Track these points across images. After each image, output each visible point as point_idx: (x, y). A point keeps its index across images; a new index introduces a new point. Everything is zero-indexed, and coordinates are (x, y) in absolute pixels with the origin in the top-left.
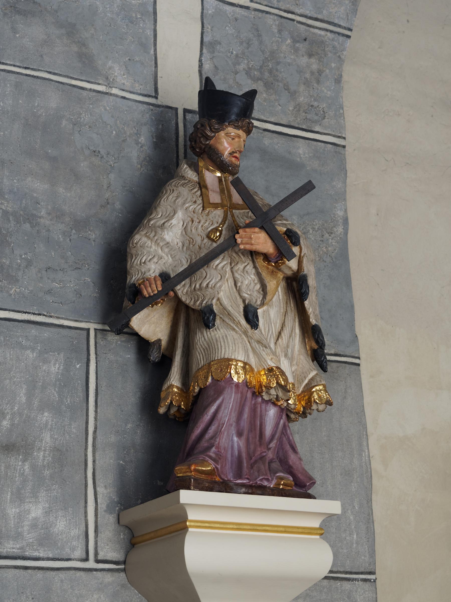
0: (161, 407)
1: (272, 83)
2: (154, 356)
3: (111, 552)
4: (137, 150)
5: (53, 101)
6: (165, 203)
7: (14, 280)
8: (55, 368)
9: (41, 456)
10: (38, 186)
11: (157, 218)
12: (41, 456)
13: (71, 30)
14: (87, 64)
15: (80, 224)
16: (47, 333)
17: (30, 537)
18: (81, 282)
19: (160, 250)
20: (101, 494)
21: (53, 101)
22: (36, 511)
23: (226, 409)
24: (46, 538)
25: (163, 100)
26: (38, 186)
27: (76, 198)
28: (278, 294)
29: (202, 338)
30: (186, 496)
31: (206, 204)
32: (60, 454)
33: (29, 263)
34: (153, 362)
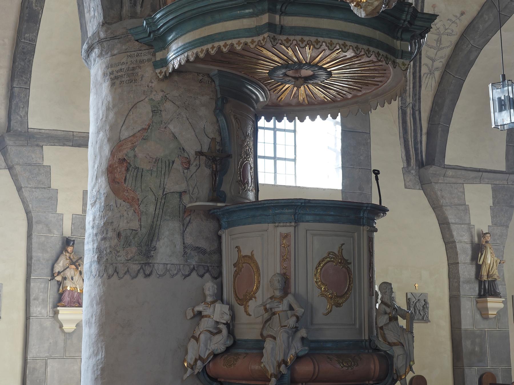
0: (451, 42)
1: (246, 44)
2: (59, 283)
3: (51, 315)
4: (58, 246)
5: (43, 239)
6: (60, 258)
7: (36, 271)
8: (43, 286)
9: (40, 300)
10: (40, 255)
11: (58, 261)
12: (40, 300)
13: (47, 225)
14: (50, 231)
15: (48, 260)
16: (41, 280)
17: (38, 313)
18: (48, 271)
19: (58, 268)
20: (50, 306)
21: (43, 239)
22: (39, 309)
23: (66, 294)
24: (41, 313)
25: (64, 235)
26: (40, 255)
27: (47, 256)
28: (78, 274)
29: (65, 282)
30: (58, 308)
31: (67, 259)
32: (43, 300)
33: (39, 268)
34: (59, 283)
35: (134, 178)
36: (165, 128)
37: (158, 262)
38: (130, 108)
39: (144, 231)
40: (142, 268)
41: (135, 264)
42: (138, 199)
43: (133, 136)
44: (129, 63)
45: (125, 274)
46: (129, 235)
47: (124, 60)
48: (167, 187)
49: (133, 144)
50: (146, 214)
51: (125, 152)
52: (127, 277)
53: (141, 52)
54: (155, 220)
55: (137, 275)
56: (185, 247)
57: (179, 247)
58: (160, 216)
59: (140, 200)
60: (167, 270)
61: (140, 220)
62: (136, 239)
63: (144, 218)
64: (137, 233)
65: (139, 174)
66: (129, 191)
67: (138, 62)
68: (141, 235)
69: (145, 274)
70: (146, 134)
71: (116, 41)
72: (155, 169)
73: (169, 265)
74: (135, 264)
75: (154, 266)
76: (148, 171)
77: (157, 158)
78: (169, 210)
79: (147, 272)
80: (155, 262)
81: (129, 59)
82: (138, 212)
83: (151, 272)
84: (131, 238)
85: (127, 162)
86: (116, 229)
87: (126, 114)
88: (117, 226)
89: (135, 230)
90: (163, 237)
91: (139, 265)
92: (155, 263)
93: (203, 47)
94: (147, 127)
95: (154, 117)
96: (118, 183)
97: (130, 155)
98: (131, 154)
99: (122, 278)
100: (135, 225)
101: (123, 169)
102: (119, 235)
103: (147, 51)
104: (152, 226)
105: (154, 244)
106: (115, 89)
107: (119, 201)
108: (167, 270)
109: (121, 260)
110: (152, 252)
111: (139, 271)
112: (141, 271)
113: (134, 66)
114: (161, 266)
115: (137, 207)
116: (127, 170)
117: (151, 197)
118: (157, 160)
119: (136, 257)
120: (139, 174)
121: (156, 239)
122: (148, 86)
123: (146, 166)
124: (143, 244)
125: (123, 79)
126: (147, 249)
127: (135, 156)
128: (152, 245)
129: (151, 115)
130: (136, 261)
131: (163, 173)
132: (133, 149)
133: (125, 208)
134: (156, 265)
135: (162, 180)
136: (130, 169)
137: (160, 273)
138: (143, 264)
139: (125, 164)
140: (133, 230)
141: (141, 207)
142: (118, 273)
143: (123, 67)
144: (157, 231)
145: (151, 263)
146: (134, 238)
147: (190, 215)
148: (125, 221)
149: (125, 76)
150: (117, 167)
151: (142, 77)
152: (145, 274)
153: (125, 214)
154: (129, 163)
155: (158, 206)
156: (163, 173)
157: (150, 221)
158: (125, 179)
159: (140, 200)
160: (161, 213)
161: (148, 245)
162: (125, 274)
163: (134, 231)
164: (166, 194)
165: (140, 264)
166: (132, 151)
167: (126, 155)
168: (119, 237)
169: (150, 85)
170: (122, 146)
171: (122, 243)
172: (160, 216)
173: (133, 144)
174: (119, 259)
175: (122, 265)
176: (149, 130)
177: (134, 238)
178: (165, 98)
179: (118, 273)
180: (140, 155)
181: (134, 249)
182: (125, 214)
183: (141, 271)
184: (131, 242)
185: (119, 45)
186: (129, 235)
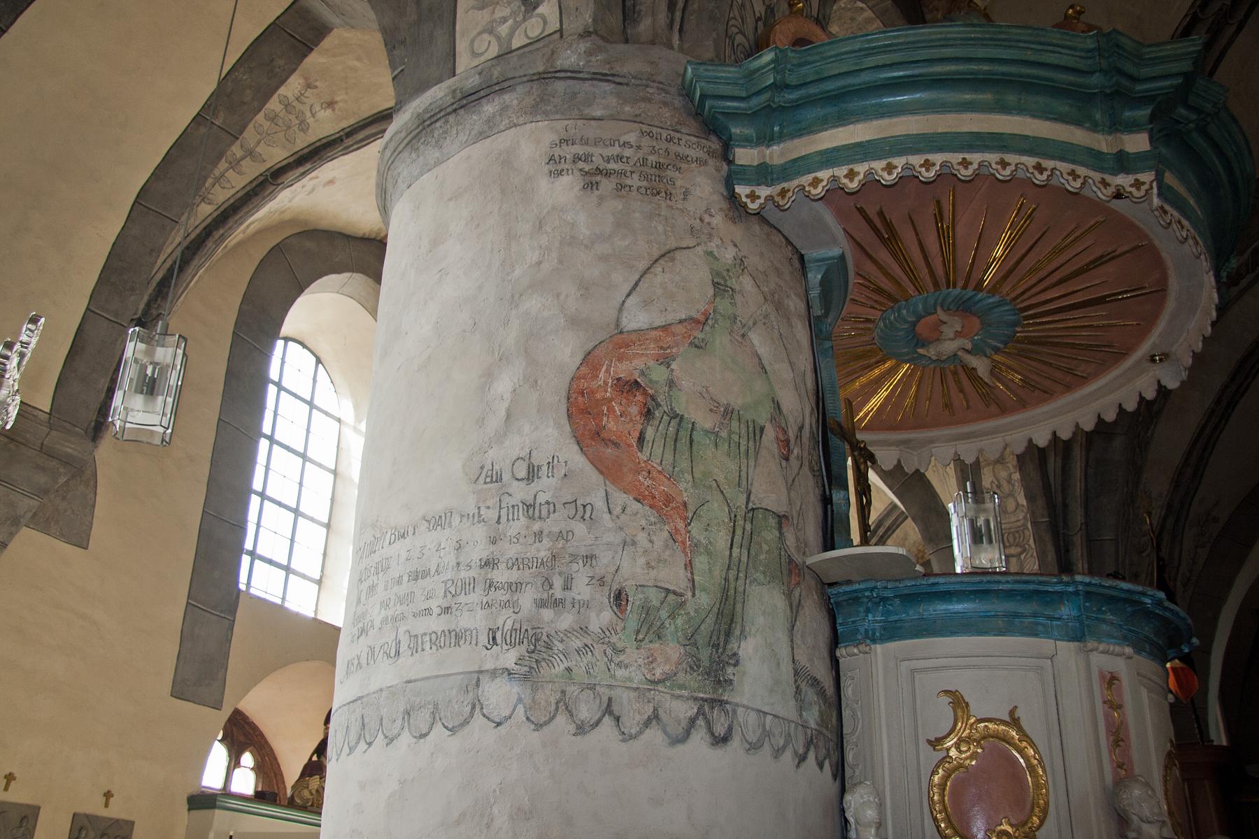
35: (670, 442)
36: (743, 336)
37: (745, 702)
38: (656, 256)
39: (704, 600)
40: (700, 712)
41: (679, 697)
42: (685, 504)
43: (665, 328)
44: (646, 150)
45: (647, 724)
46: (656, 603)
47: (632, 138)
48: (753, 490)
49: (662, 348)
50: (709, 553)
51: (639, 363)
52: (654, 735)
53: (678, 135)
54: (732, 574)
55: (687, 734)
56: (796, 673)
57: (787, 669)
58: (743, 568)
59: (691, 508)
60: (767, 734)
61: (689, 565)
62: (679, 621)
63: (701, 562)
64: (682, 605)
65: (684, 435)
66: (654, 474)
67: (672, 155)
68: (696, 611)
69: (713, 734)
70: (701, 336)
71: (607, 87)
72: (724, 434)
73: (769, 718)
74: (679, 697)
75: (734, 712)
76: (707, 432)
77: (728, 405)
78: (762, 557)
79: (720, 730)
80: (737, 700)
81: (646, 142)
82: (683, 543)
83: (730, 729)
84: (664, 614)
85: (645, 393)
86: (608, 578)
87: (642, 265)
88: (613, 569)
89: (675, 593)
90: (753, 631)
91: (691, 703)
92: (737, 705)
93: (931, 157)
94: (702, 318)
95: (718, 299)
96: (616, 445)
97: (654, 377)
98: (659, 374)
99: (632, 737)
100: (675, 576)
101: (634, 410)
102: (619, 598)
103: (695, 139)
104: (725, 591)
105: (733, 645)
106: (601, 199)
107: (619, 498)
108: (767, 734)
109: (630, 679)
110: (730, 670)
111: (692, 721)
112: (701, 722)
113: (661, 160)
114: (752, 717)
115: (681, 525)
116: (648, 414)
117: (717, 510)
118: (728, 412)
119: (681, 675)
120: (684, 435)
121: (737, 632)
122: (701, 220)
123: (705, 420)
124: (701, 641)
125: (629, 182)
126: (714, 659)
127: (671, 384)
128: (729, 647)
129: (711, 292)
130: (682, 687)
131: (743, 449)
132: (666, 361)
133: (643, 522)
134: (740, 711)
135: (744, 468)
136: (657, 414)
137: (752, 738)
138: (706, 700)
139: (639, 398)
140: (668, 591)
141: (695, 528)
142: (618, 719)
143: (628, 152)
144: (739, 606)
145: (727, 702)
146: (672, 616)
147: (798, 583)
148: (642, 561)
149: (635, 176)
150: (610, 400)
151: (686, 194)
152: (713, 734)
153: (642, 538)
154: (653, 398)
155: (737, 538)
156: (743, 449)
157: (718, 573)
158: (641, 439)
159: (691, 508)
160: (744, 559)
161: (716, 646)
162: (647, 724)
163: (671, 597)
164: (753, 509)
165: (696, 699)
166: (663, 368)
167: (642, 373)
168: (619, 606)
169: (707, 219)
170: (628, 346)
171: (632, 624)
172: (743, 568)
173: (662, 348)
174: (620, 673)
175: (633, 694)
176: (707, 328)
177: (672, 616)
178: (741, 262)
179: (618, 719)
180: (685, 384)
181: (671, 652)
182: (642, 538)
183: (701, 722)
184: (662, 625)
185: (613, 101)
186: (656, 603)
